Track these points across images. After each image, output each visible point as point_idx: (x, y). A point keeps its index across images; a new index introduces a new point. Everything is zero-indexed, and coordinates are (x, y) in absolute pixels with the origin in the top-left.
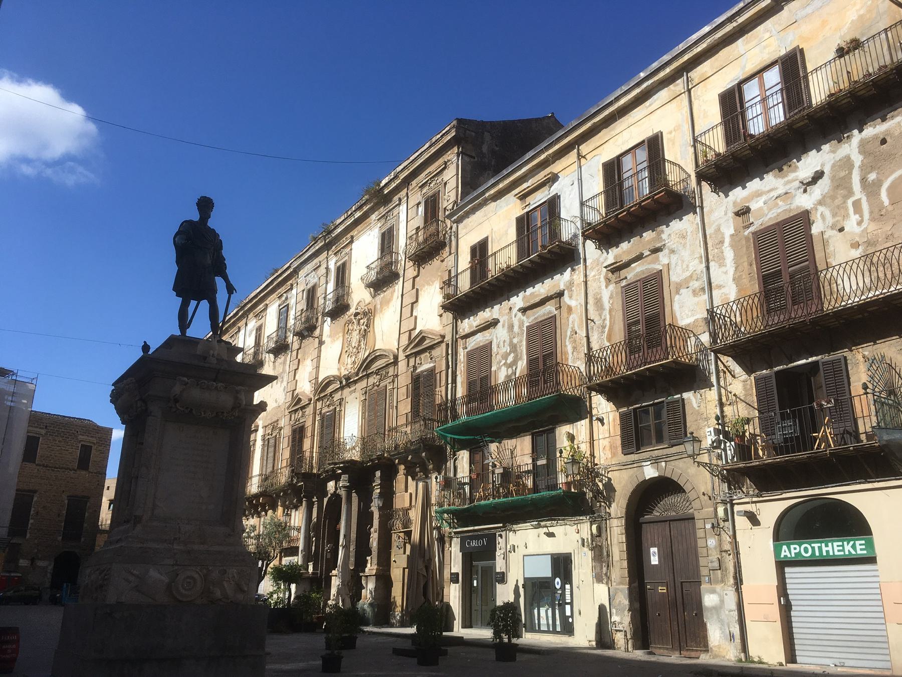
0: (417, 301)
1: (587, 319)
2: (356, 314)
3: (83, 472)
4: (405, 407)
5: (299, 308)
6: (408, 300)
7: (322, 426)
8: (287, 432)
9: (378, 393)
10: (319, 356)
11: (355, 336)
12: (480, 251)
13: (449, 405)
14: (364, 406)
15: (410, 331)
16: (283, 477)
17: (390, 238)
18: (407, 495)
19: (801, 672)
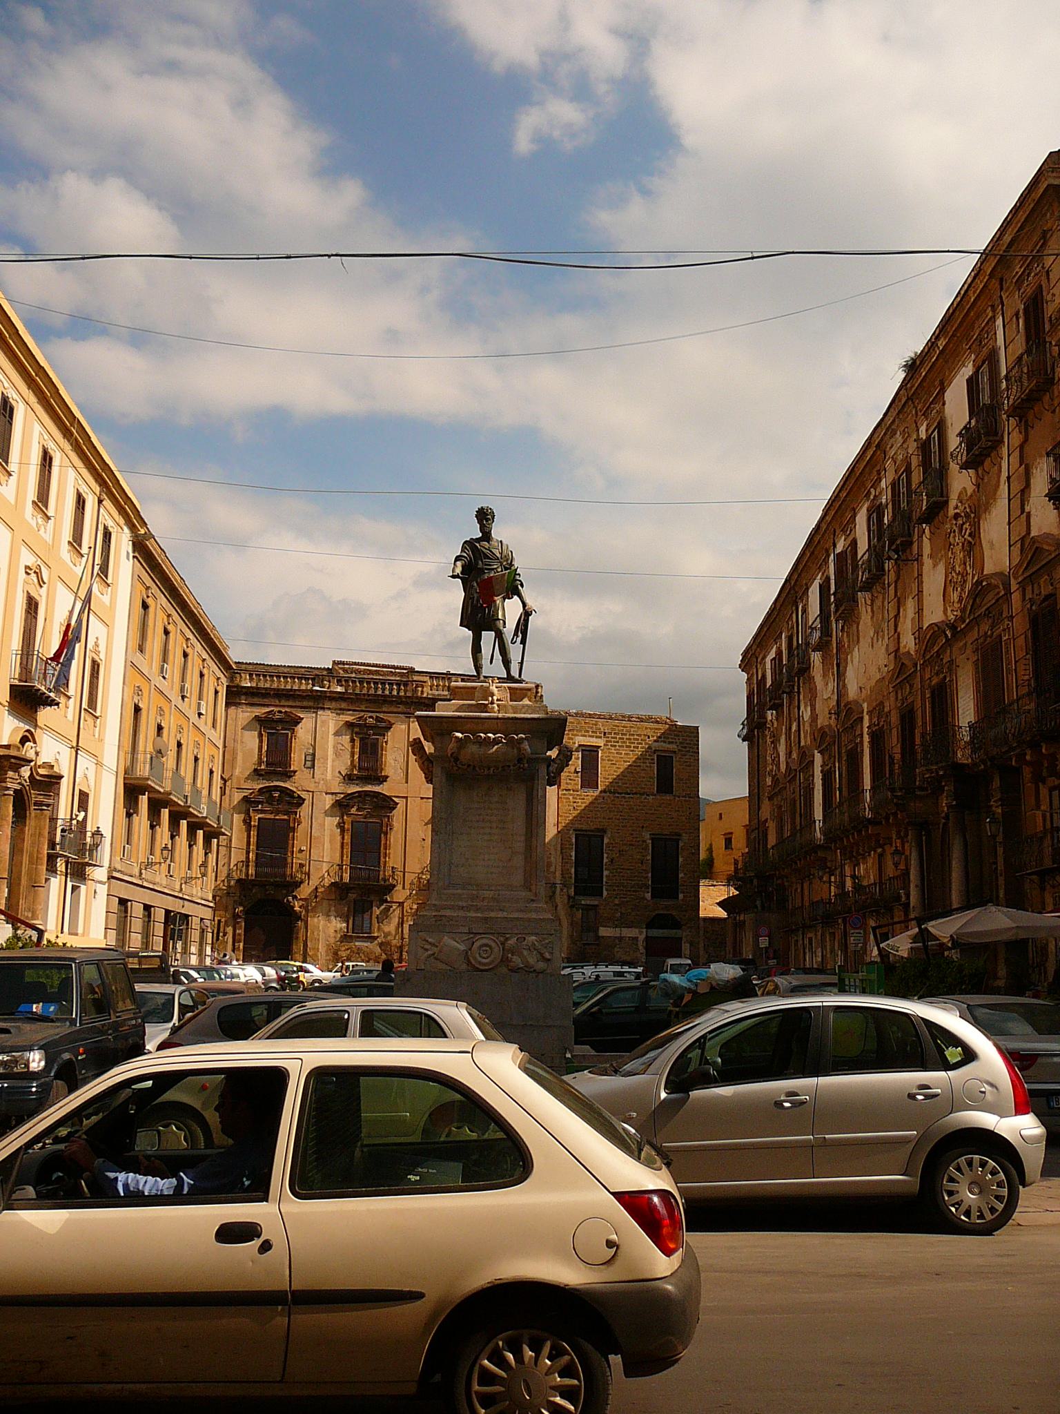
0: (1028, 485)
3: (668, 797)
6: (1016, 487)
8: (895, 719)
10: (920, 592)
15: (1023, 539)
18: (1039, 813)
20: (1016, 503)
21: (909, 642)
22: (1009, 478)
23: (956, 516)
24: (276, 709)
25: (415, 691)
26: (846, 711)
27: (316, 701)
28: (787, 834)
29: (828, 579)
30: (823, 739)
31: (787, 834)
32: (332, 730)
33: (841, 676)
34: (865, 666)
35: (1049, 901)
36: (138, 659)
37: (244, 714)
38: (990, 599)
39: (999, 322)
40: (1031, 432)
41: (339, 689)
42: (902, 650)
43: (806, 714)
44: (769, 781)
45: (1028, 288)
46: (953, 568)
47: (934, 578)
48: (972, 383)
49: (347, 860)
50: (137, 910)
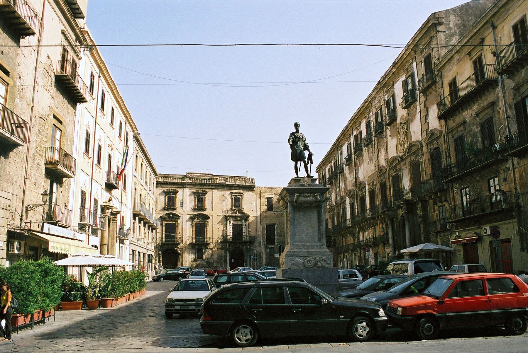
0: (428, 113)
6: (423, 114)
8: (378, 186)
10: (387, 147)
12: (453, 85)
14: (410, 171)
15: (426, 130)
19: (349, 306)
20: (423, 119)
21: (383, 163)
22: (420, 112)
23: (401, 123)
24: (170, 188)
25: (214, 182)
26: (359, 185)
27: (183, 185)
28: (336, 224)
29: (350, 143)
30: (350, 194)
31: (336, 224)
32: (188, 194)
33: (356, 173)
34: (366, 170)
35: (439, 240)
36: (135, 173)
37: (160, 190)
38: (414, 149)
39: (414, 64)
40: (428, 98)
41: (191, 181)
42: (380, 165)
43: (343, 185)
44: (328, 207)
45: (426, 53)
46: (400, 140)
47: (392, 143)
48: (405, 83)
49: (194, 236)
50: (142, 255)
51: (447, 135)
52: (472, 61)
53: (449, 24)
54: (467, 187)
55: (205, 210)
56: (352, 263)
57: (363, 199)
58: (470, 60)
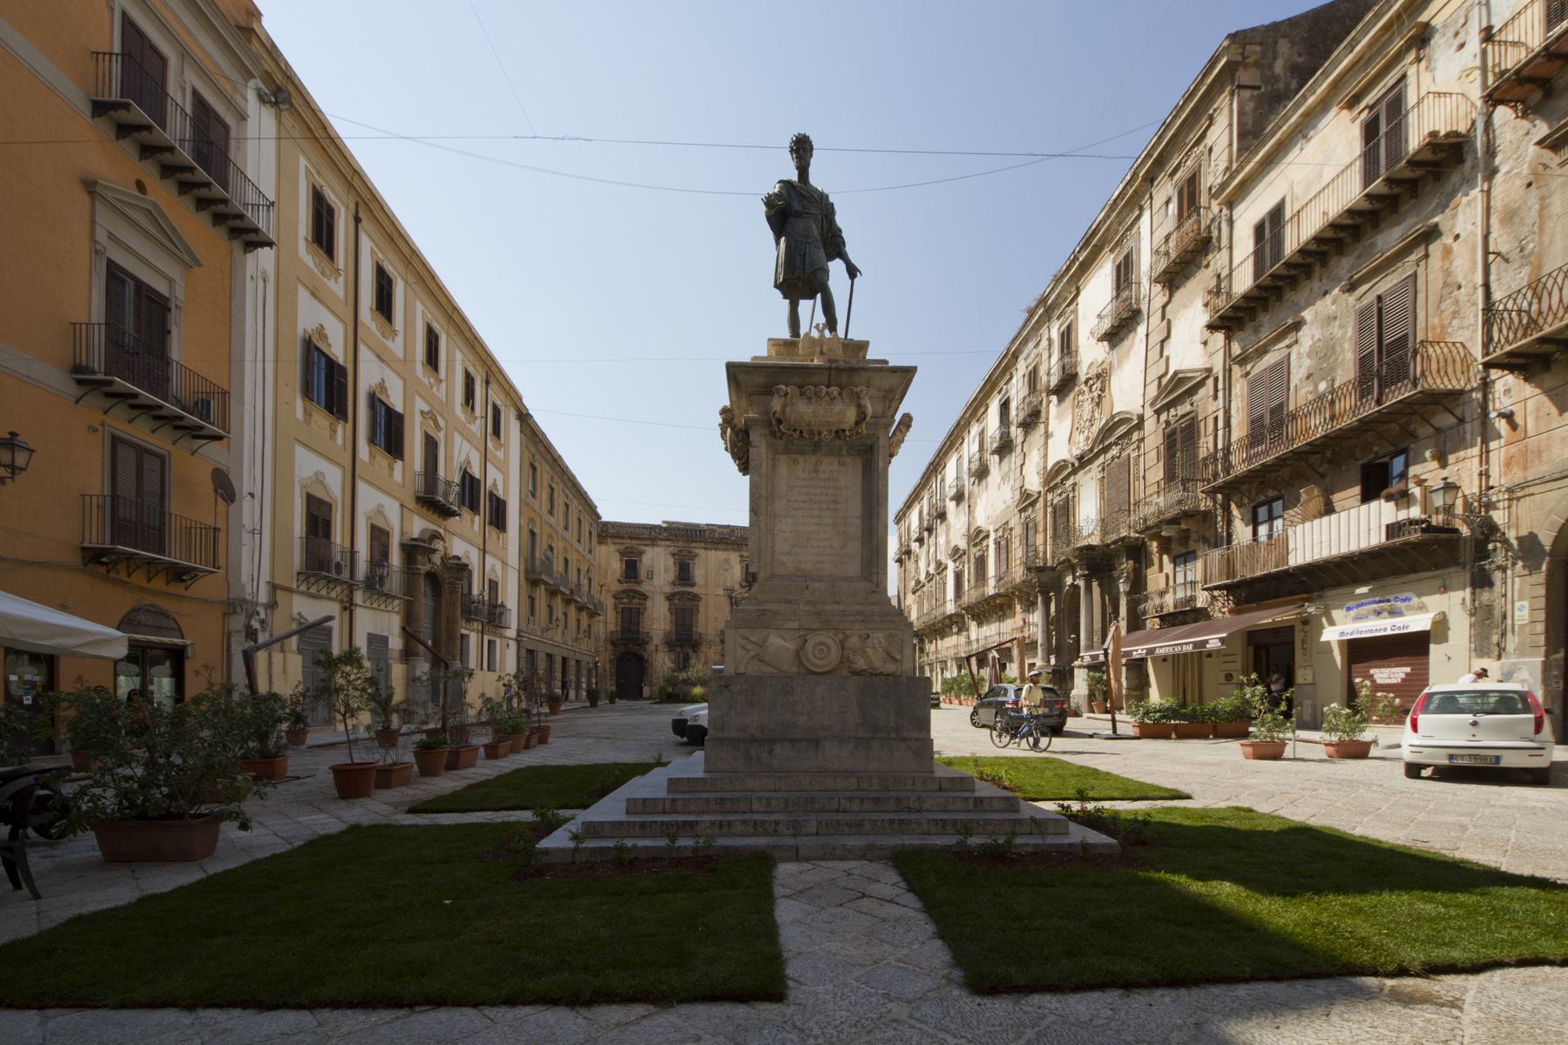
1: (1486, 253)
2: (1086, 382)
4: (1156, 474)
5: (1021, 395)
6: (1155, 338)
7: (1055, 518)
8: (1018, 531)
9: (1119, 466)
11: (1087, 406)
13: (1220, 454)
16: (1018, 573)
17: (1126, 274)
26: (977, 537)
50: (572, 663)
51: (1228, 372)
52: (1358, 122)
53: (1271, 67)
54: (1277, 499)
55: (694, 585)
56: (178, 675)
57: (981, 563)
58: (1353, 121)
